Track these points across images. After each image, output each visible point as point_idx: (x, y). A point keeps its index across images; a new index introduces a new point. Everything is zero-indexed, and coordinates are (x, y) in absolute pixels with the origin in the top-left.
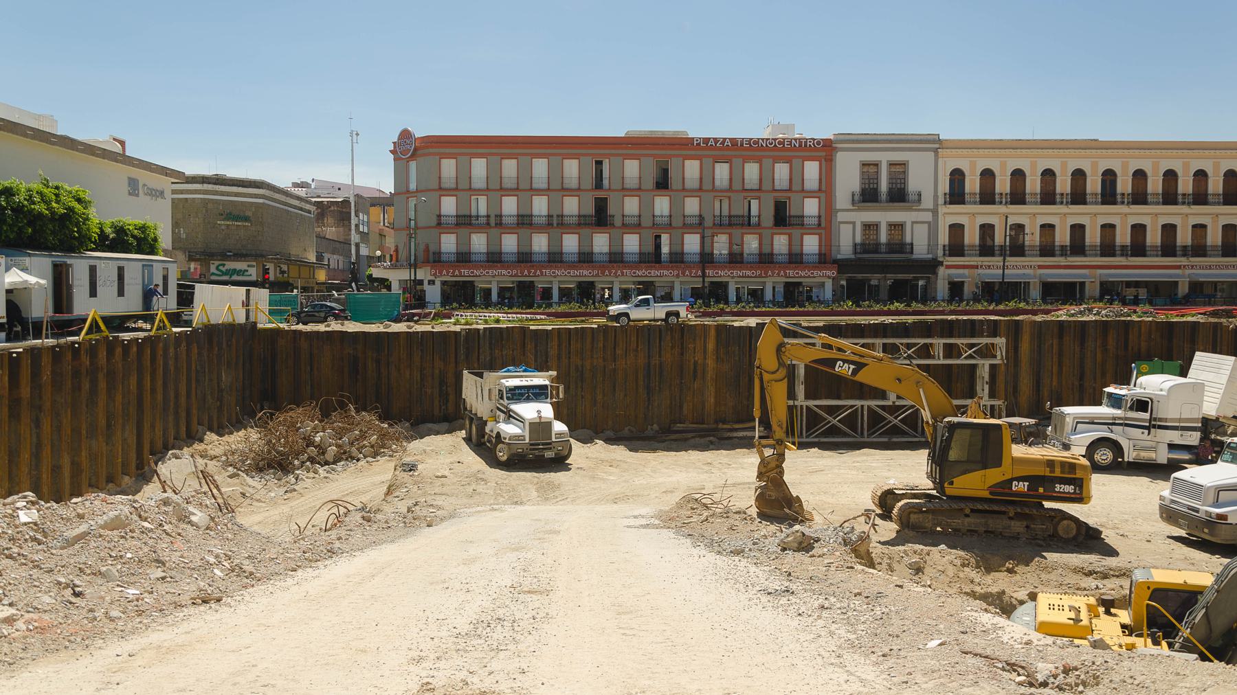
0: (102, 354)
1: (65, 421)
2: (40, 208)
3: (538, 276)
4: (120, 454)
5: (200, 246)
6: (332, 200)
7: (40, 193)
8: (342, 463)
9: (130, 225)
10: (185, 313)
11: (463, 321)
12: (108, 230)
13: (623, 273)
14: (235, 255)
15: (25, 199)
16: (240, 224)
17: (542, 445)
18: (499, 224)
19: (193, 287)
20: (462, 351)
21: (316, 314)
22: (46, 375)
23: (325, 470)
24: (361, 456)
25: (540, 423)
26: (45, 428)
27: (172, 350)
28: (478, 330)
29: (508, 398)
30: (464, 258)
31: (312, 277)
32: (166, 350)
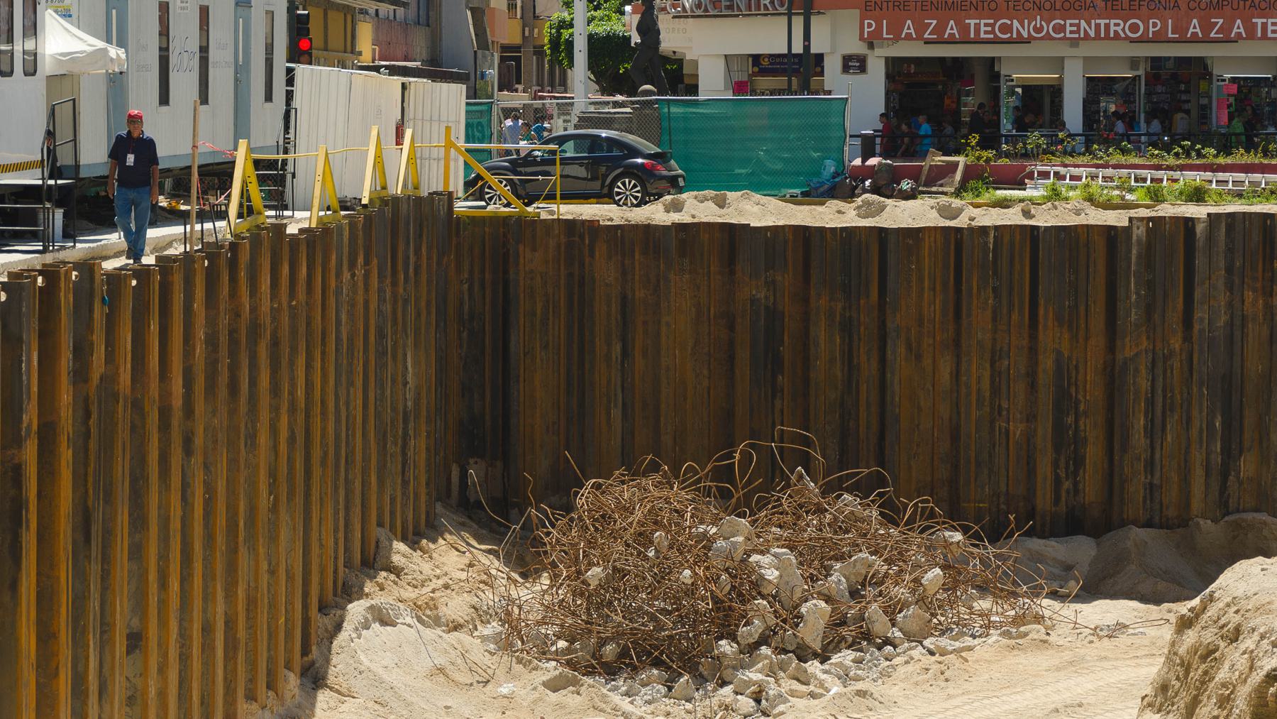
20: (1132, 292)
28: (1189, 222)
31: (349, 48)
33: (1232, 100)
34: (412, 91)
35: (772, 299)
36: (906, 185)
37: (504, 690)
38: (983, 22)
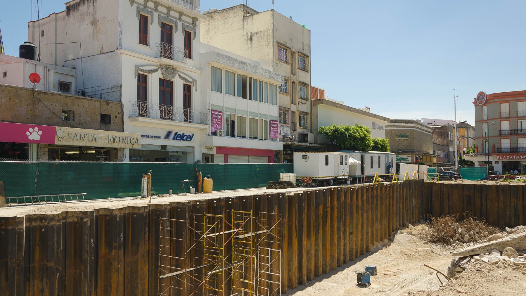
1: (369, 215)
2: (357, 135)
6: (436, 127)
9: (379, 140)
16: (404, 139)
21: (445, 176)
31: (431, 161)
34: (420, 167)
37: (418, 244)
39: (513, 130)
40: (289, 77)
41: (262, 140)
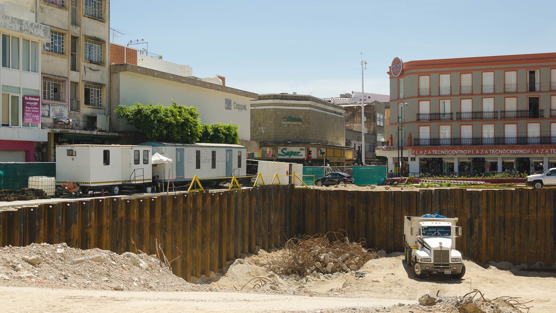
0: (200, 201)
1: (178, 237)
2: (171, 119)
3: (486, 154)
4: (209, 258)
5: (272, 138)
7: (171, 111)
8: (337, 273)
9: (221, 127)
10: (253, 178)
11: (426, 185)
12: (210, 130)
13: (550, 152)
14: (292, 143)
15: (164, 115)
17: (443, 265)
18: (459, 119)
19: (257, 163)
21: (334, 180)
22: (169, 211)
23: (324, 277)
24: (349, 269)
25: (441, 251)
26: (168, 240)
27: (240, 200)
28: (431, 191)
29: (423, 234)
30: (435, 142)
32: (236, 199)
33: (490, 166)
35: (353, 205)
36: (396, 183)
38: (493, 150)
39: (434, 114)
40: (67, 29)
41: (8, 125)
